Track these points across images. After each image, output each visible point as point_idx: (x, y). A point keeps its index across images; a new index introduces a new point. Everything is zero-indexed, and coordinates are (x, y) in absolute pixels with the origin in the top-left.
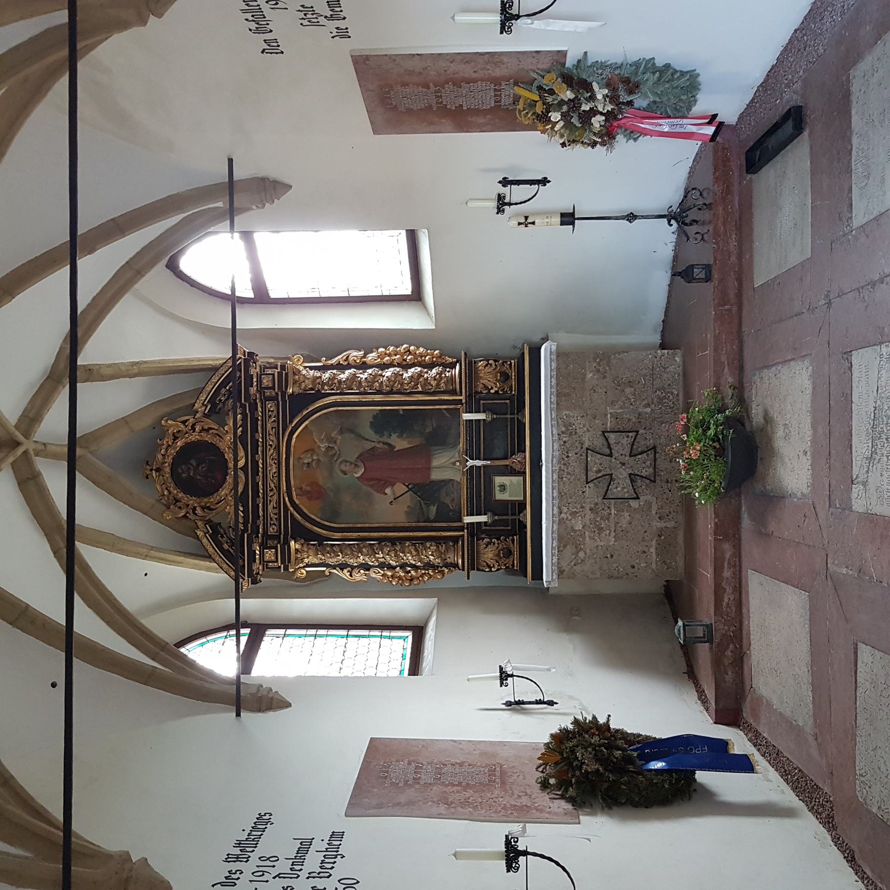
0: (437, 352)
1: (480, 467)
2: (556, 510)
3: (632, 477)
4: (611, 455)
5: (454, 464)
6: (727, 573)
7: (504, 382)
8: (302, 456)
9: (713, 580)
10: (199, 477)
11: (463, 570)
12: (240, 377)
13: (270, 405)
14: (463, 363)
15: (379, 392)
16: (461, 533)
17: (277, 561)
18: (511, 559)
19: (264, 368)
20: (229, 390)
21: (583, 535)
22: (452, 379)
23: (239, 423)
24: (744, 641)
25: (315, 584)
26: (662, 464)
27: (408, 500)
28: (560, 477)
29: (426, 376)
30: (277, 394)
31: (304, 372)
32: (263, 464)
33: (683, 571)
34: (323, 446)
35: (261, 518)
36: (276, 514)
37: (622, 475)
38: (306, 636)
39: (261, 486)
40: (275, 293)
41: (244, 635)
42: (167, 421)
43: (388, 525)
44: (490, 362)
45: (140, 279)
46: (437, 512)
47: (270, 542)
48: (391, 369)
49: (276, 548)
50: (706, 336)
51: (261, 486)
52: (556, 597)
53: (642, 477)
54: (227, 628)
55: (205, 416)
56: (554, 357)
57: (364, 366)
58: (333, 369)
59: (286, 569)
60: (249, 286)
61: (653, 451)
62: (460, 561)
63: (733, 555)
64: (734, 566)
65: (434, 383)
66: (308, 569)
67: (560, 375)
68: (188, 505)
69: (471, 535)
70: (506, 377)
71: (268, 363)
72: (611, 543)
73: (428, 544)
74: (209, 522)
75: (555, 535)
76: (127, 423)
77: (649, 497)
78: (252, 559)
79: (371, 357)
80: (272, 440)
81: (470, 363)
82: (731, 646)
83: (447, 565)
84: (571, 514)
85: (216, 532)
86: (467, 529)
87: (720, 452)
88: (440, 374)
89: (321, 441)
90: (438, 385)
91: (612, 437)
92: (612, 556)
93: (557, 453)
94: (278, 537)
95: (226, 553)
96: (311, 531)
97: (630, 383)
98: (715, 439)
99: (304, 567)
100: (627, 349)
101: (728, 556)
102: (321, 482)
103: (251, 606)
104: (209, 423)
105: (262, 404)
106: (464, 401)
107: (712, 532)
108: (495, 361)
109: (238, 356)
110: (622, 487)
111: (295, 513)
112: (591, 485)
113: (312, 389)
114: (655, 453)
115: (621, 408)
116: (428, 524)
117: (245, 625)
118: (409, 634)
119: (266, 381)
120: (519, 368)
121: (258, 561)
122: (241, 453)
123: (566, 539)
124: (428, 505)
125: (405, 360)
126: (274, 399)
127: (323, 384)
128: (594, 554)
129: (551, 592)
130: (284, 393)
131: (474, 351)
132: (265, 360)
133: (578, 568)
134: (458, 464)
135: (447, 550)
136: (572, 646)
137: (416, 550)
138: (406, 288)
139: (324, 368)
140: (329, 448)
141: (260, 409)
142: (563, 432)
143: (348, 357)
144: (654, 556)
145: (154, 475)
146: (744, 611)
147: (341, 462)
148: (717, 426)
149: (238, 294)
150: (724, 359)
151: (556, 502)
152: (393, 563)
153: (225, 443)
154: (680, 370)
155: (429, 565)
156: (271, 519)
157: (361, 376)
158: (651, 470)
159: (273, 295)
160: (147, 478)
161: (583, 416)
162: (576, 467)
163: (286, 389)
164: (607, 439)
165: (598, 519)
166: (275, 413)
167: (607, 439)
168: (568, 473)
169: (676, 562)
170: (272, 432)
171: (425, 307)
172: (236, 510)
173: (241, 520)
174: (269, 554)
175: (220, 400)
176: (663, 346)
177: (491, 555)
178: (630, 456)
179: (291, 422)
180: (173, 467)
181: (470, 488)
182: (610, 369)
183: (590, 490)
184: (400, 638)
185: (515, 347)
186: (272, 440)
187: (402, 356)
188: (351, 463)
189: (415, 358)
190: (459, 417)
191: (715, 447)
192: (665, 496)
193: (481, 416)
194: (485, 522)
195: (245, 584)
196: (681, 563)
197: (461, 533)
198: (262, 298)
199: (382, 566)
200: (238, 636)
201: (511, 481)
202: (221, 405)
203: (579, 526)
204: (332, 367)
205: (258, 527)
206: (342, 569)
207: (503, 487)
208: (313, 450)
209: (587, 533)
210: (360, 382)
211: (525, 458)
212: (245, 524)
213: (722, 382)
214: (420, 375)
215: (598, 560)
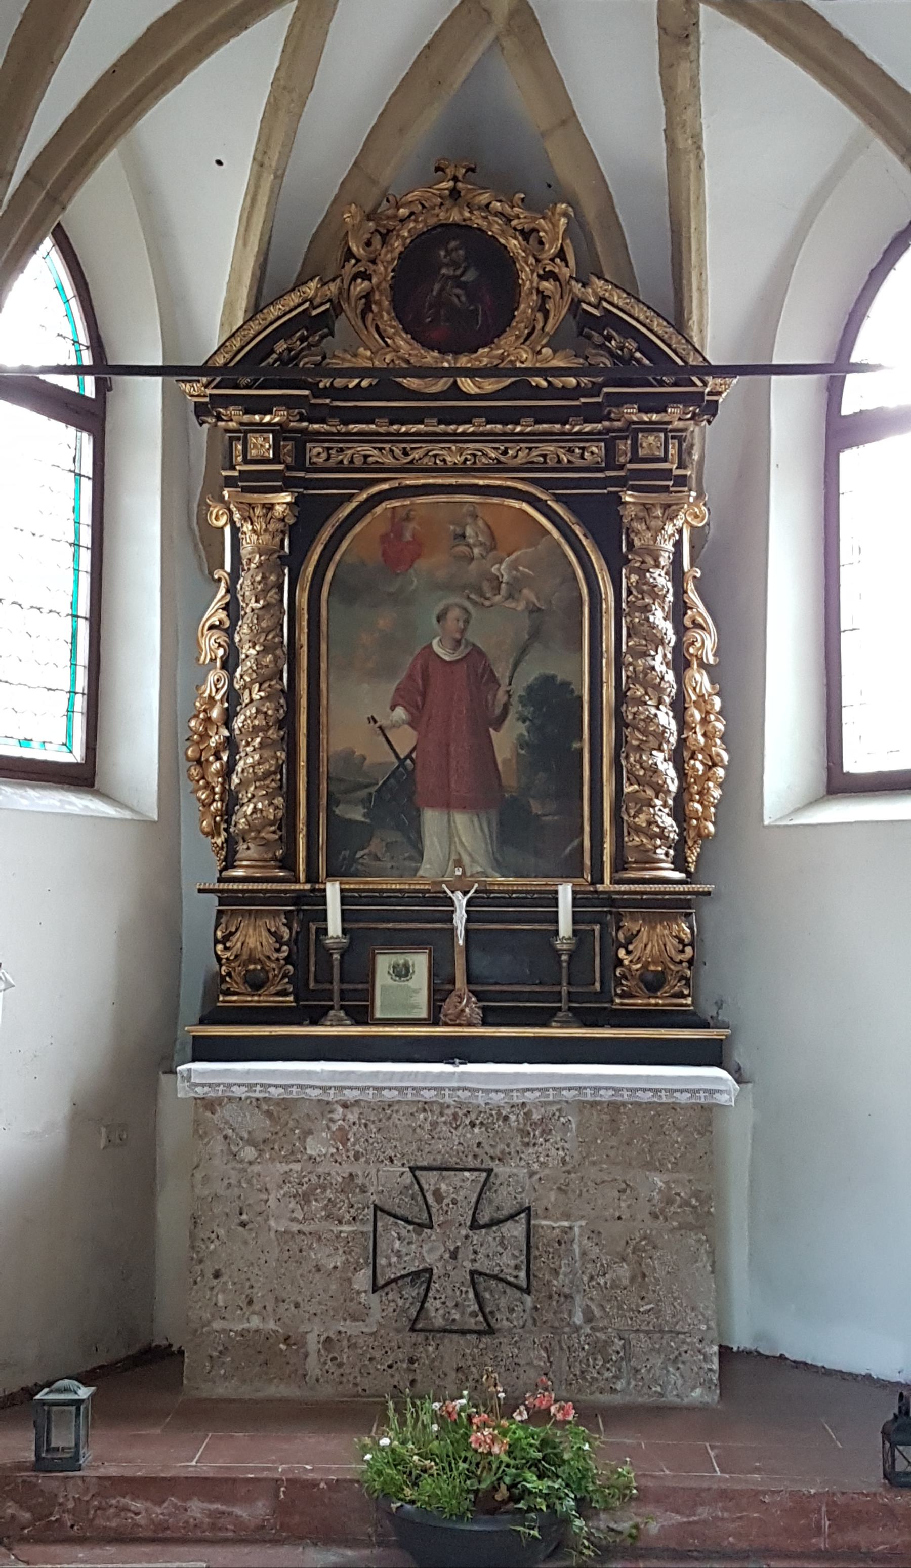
0: (711, 828)
1: (451, 920)
2: (351, 1095)
3: (423, 1277)
4: (475, 1225)
5: (459, 863)
6: (197, 1508)
7: (642, 979)
8: (480, 523)
9: (183, 1474)
10: (437, 287)
11: (220, 880)
12: (662, 383)
13: (597, 450)
14: (686, 888)
15: (621, 696)
16: (302, 876)
17: (246, 461)
18: (243, 989)
19: (679, 436)
20: (632, 357)
21: (292, 1156)
22: (650, 862)
23: (558, 382)
24: (39, 1549)
25: (194, 546)
26: (453, 1350)
27: (378, 756)
28: (425, 1107)
29: (658, 802)
30: (621, 467)
31: (670, 529)
32: (463, 434)
33: (204, 1395)
34: (502, 570)
35: (343, 429)
36: (351, 462)
37: (430, 1252)
38: (77, 523)
39: (414, 428)
40: (851, 461)
41: (81, 384)
42: (565, 214)
43: (323, 710)
44: (689, 950)
45: (895, 150)
46: (350, 821)
47: (288, 447)
48: (673, 726)
49: (276, 460)
50: (757, 1470)
51: (414, 428)
52: (152, 1092)
53: (423, 1302)
54: (97, 344)
55: (575, 304)
56: (702, 1099)
57: (681, 663)
58: (675, 595)
59: (229, 482)
60: (869, 405)
61: (483, 1326)
62: (240, 873)
63: (239, 1524)
64: (213, 1527)
65: (641, 820)
66: (228, 531)
67: (659, 1113)
68: (373, 262)
69: (298, 899)
70: (654, 984)
71: (692, 446)
72: (272, 1223)
73: (279, 801)
74: (336, 309)
75: (294, 1093)
76: (564, 123)
77: (376, 1314)
78: (252, 405)
79: (700, 680)
80: (519, 455)
81: (688, 904)
82: (28, 1515)
83: (231, 843)
84: (341, 1128)
85: (314, 324)
86: (313, 890)
87: (485, 1504)
88: (662, 836)
89: (514, 566)
90: (638, 830)
91: (516, 1230)
92: (243, 1225)
93: (481, 1099)
94: (300, 466)
95: (265, 347)
96: (311, 541)
97: (640, 1276)
98: (517, 1493)
99: (233, 523)
100: (718, 1269)
101: (238, 1511)
102: (422, 564)
103: (145, 405)
104: (558, 312)
105: (600, 433)
106: (600, 888)
107: (296, 1474)
108: (691, 962)
109: (710, 379)
110: (403, 1250)
111: (354, 505)
112: (408, 1178)
113: (630, 545)
114: (479, 1333)
115: (584, 1254)
116: (324, 801)
117: (102, 387)
118: (77, 755)
119: (650, 443)
120: (674, 1016)
121: (246, 418)
122: (490, 385)
123: (284, 1115)
124: (365, 802)
125: (692, 757)
126: (610, 461)
127: (642, 572)
128: (249, 1182)
129: (164, 1078)
130: (621, 482)
131: (710, 911)
132: (697, 442)
133: (218, 1146)
134: (458, 872)
135: (266, 844)
136: (38, 1129)
137: (267, 775)
138: (856, 761)
139: (677, 574)
140: (496, 582)
141: (588, 427)
142: (528, 1115)
143: (701, 627)
144: (239, 1327)
145: (444, 185)
146: (111, 1550)
147: (465, 610)
148: (546, 1496)
149: (851, 379)
150: (703, 1513)
151: (370, 1096)
152: (238, 723)
153: (514, 350)
154: (671, 1398)
155: (231, 801)
156: (341, 450)
157: (659, 658)
158: (439, 1322)
159: (848, 459)
160: (438, 169)
161: (564, 1162)
162: (450, 1143)
163: (633, 488)
164: (511, 1217)
165: (329, 1194)
166: (579, 462)
167: (511, 1217)
168: (434, 1124)
169: (225, 1377)
170: (535, 457)
171: (813, 802)
172: (362, 373)
173: (339, 382)
174: (262, 445)
175: (609, 338)
176: (725, 1352)
177: (252, 942)
178: (472, 1273)
179: (558, 498)
180: (462, 229)
181: (401, 897)
182: (673, 1230)
183: (396, 1175)
184: (69, 735)
185: (720, 1005)
186: (519, 455)
187: (702, 750)
188: (463, 631)
189: (697, 778)
190: (566, 876)
191: (495, 1488)
192: (378, 1355)
193: (565, 926)
194: (325, 931)
195: (195, 389)
196: (222, 1390)
197: (302, 876)
198: (840, 432)
199: (233, 697)
200: (79, 370)
201: (416, 991)
202: (597, 338)
203: (314, 1147)
204: (679, 591)
205: (323, 421)
206: (226, 608)
207: (403, 972)
208: (493, 548)
209: (297, 1167)
210: (645, 655)
211: (470, 1025)
212: (331, 392)
213: (649, 1509)
214: (659, 790)
215: (236, 1192)
